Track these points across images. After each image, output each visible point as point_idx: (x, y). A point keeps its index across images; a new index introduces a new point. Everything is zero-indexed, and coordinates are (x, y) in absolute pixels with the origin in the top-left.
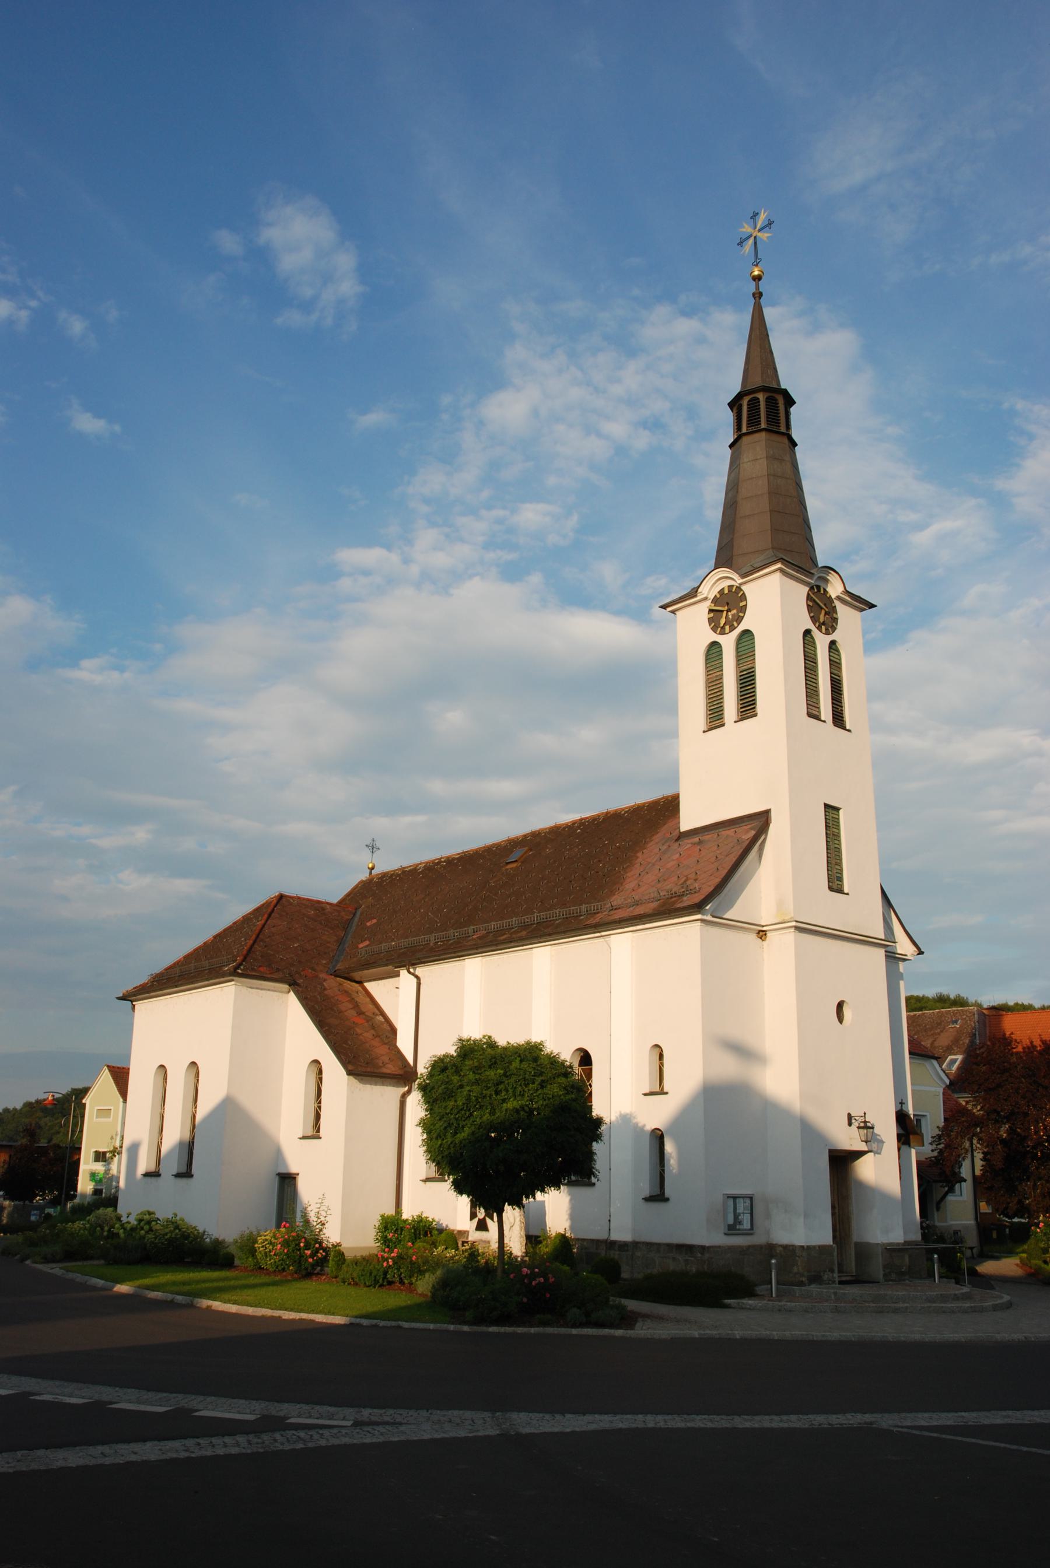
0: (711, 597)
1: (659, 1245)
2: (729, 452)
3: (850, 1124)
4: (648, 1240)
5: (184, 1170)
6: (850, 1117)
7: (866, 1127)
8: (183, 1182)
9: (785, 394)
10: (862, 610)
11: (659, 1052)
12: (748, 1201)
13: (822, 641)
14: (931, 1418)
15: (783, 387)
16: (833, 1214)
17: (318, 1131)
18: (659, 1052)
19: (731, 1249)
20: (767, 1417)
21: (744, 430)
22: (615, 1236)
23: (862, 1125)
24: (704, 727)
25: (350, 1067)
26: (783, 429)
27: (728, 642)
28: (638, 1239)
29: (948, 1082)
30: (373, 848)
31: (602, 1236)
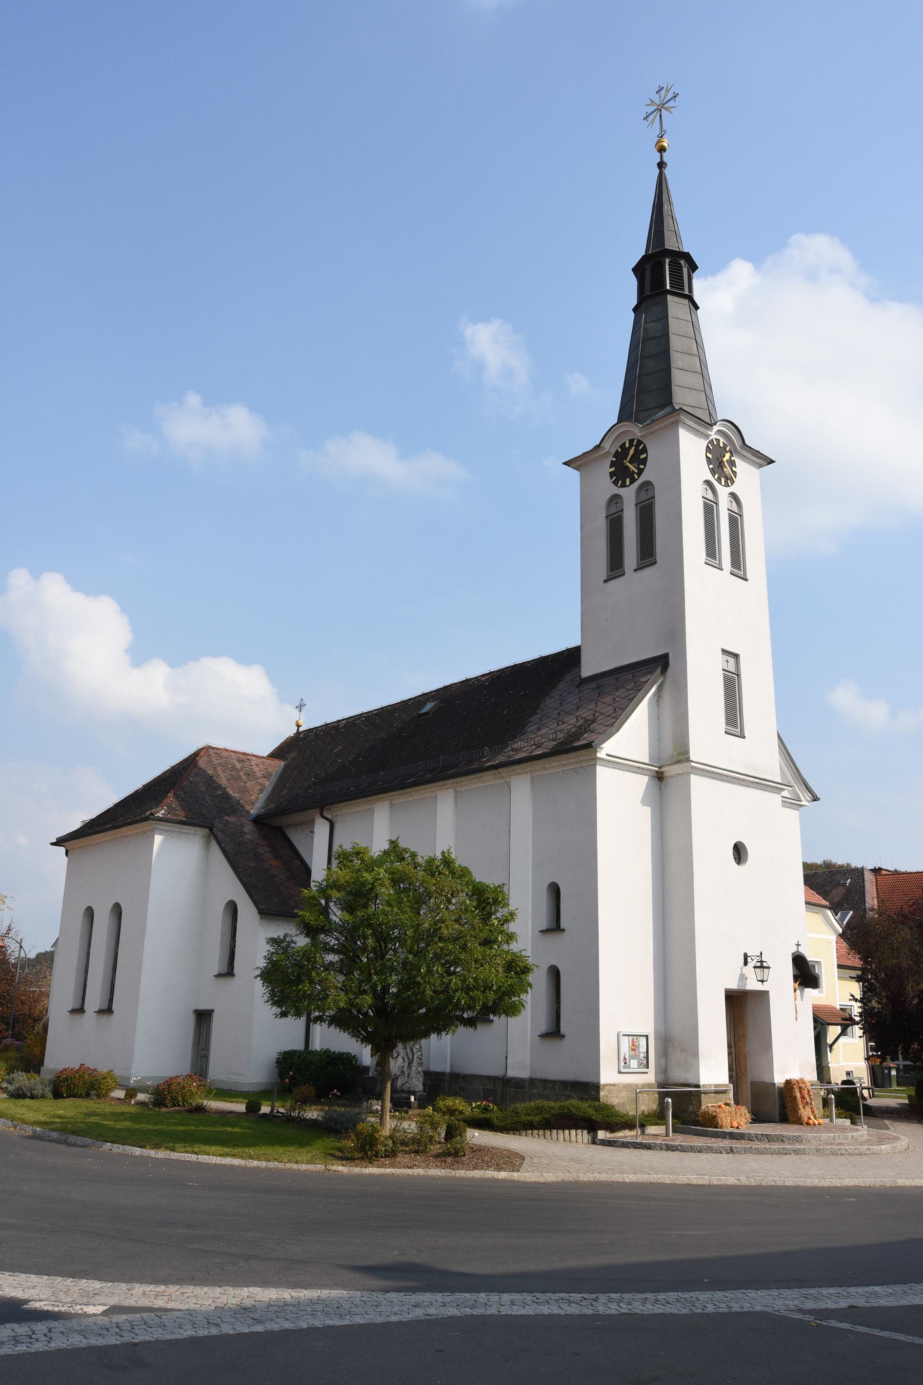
0: (613, 451)
1: (554, 1082)
2: (632, 315)
3: (746, 963)
4: (570, 1077)
5: (78, 1006)
6: (746, 957)
7: (762, 967)
8: (104, 1018)
9: (687, 257)
10: (761, 466)
11: (555, 891)
12: (644, 1039)
13: (723, 492)
14: (838, 1295)
15: (685, 251)
16: (730, 1054)
17: (233, 969)
18: (555, 891)
19: (627, 1087)
20: (639, 1296)
21: (647, 293)
22: (511, 1073)
23: (759, 964)
24: (605, 577)
25: (261, 907)
26: (687, 292)
27: (629, 494)
28: (533, 1076)
29: (841, 931)
30: (300, 707)
31: (497, 1072)
